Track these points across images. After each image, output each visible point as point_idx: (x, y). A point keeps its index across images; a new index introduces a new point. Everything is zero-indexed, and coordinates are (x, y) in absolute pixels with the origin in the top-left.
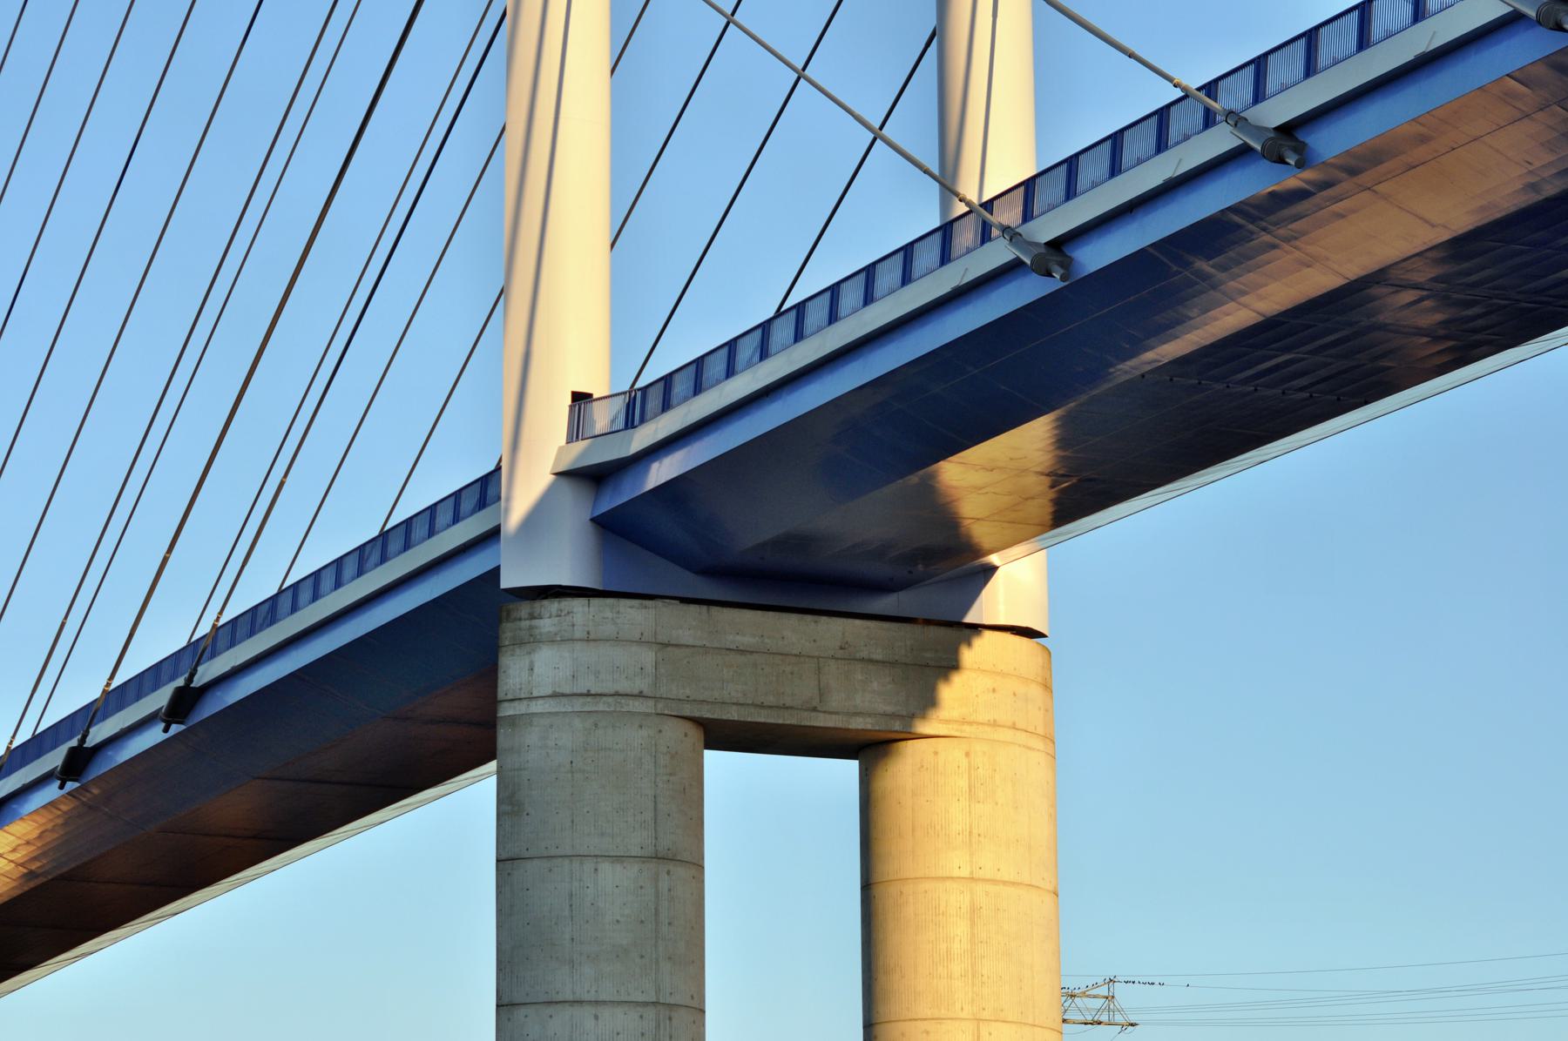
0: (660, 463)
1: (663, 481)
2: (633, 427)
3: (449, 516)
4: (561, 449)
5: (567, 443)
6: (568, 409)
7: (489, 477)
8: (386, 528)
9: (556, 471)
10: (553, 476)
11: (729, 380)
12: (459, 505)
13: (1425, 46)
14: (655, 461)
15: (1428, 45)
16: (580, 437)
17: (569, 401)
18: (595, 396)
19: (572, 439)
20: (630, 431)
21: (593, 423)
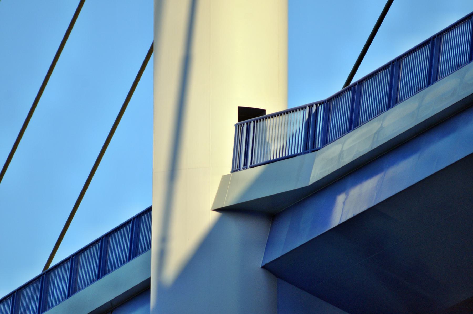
0: (347, 194)
1: (350, 216)
2: (315, 150)
3: (93, 268)
4: (225, 179)
5: (233, 171)
6: (234, 128)
7: (333, 103)
8: (356, 79)
9: (228, 202)
10: (216, 214)
11: (431, 87)
12: (76, 273)
13: (339, 221)
14: (340, 193)
15: (340, 222)
16: (249, 164)
17: (235, 120)
18: (268, 113)
19: (240, 166)
20: (309, 156)
21: (266, 147)
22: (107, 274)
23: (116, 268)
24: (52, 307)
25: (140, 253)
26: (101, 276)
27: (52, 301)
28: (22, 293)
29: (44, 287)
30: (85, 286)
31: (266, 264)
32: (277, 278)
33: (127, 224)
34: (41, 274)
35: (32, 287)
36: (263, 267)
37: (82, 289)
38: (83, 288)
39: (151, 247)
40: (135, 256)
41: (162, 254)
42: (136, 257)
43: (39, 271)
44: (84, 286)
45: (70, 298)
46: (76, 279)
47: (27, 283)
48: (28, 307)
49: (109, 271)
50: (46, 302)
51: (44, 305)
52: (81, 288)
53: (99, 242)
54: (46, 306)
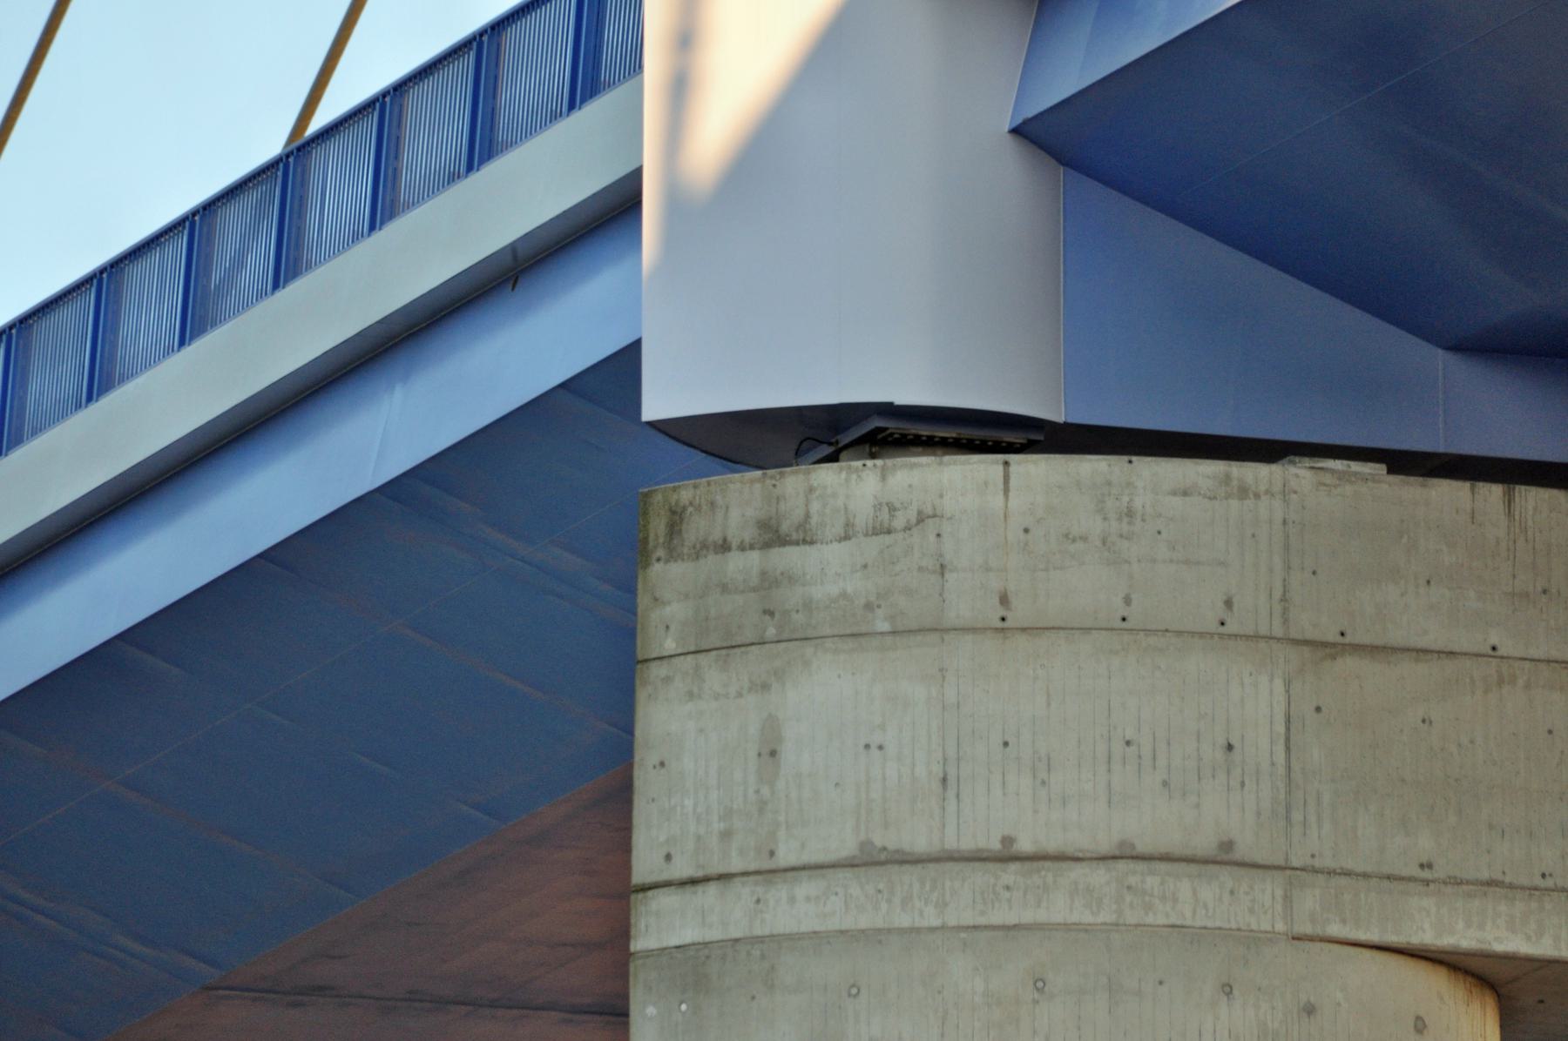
22: (497, 154)
23: (54, 423)
24: (319, 263)
25: (558, 115)
26: (581, 99)
27: (319, 244)
28: (504, 38)
29: (292, 196)
30: (426, 196)
31: (1027, 122)
32: (1062, 168)
33: (526, 10)
34: (280, 155)
35: (252, 197)
36: (1016, 131)
37: (130, 379)
38: (418, 201)
39: (641, 67)
40: (591, 97)
41: (681, 88)
42: (491, 161)
43: (271, 146)
44: (334, 251)
45: (93, 406)
46: (396, 173)
47: (438, 55)
48: (239, 263)
49: (504, 147)
50: (299, 245)
51: (291, 257)
52: (413, 202)
53: (471, 49)
54: (297, 260)
